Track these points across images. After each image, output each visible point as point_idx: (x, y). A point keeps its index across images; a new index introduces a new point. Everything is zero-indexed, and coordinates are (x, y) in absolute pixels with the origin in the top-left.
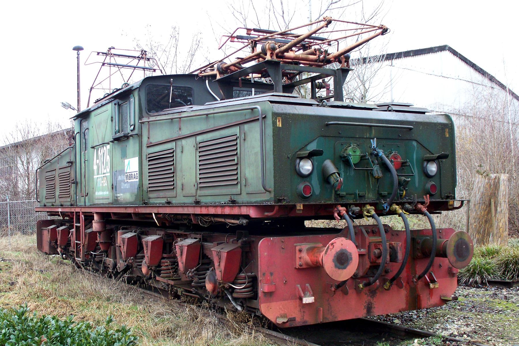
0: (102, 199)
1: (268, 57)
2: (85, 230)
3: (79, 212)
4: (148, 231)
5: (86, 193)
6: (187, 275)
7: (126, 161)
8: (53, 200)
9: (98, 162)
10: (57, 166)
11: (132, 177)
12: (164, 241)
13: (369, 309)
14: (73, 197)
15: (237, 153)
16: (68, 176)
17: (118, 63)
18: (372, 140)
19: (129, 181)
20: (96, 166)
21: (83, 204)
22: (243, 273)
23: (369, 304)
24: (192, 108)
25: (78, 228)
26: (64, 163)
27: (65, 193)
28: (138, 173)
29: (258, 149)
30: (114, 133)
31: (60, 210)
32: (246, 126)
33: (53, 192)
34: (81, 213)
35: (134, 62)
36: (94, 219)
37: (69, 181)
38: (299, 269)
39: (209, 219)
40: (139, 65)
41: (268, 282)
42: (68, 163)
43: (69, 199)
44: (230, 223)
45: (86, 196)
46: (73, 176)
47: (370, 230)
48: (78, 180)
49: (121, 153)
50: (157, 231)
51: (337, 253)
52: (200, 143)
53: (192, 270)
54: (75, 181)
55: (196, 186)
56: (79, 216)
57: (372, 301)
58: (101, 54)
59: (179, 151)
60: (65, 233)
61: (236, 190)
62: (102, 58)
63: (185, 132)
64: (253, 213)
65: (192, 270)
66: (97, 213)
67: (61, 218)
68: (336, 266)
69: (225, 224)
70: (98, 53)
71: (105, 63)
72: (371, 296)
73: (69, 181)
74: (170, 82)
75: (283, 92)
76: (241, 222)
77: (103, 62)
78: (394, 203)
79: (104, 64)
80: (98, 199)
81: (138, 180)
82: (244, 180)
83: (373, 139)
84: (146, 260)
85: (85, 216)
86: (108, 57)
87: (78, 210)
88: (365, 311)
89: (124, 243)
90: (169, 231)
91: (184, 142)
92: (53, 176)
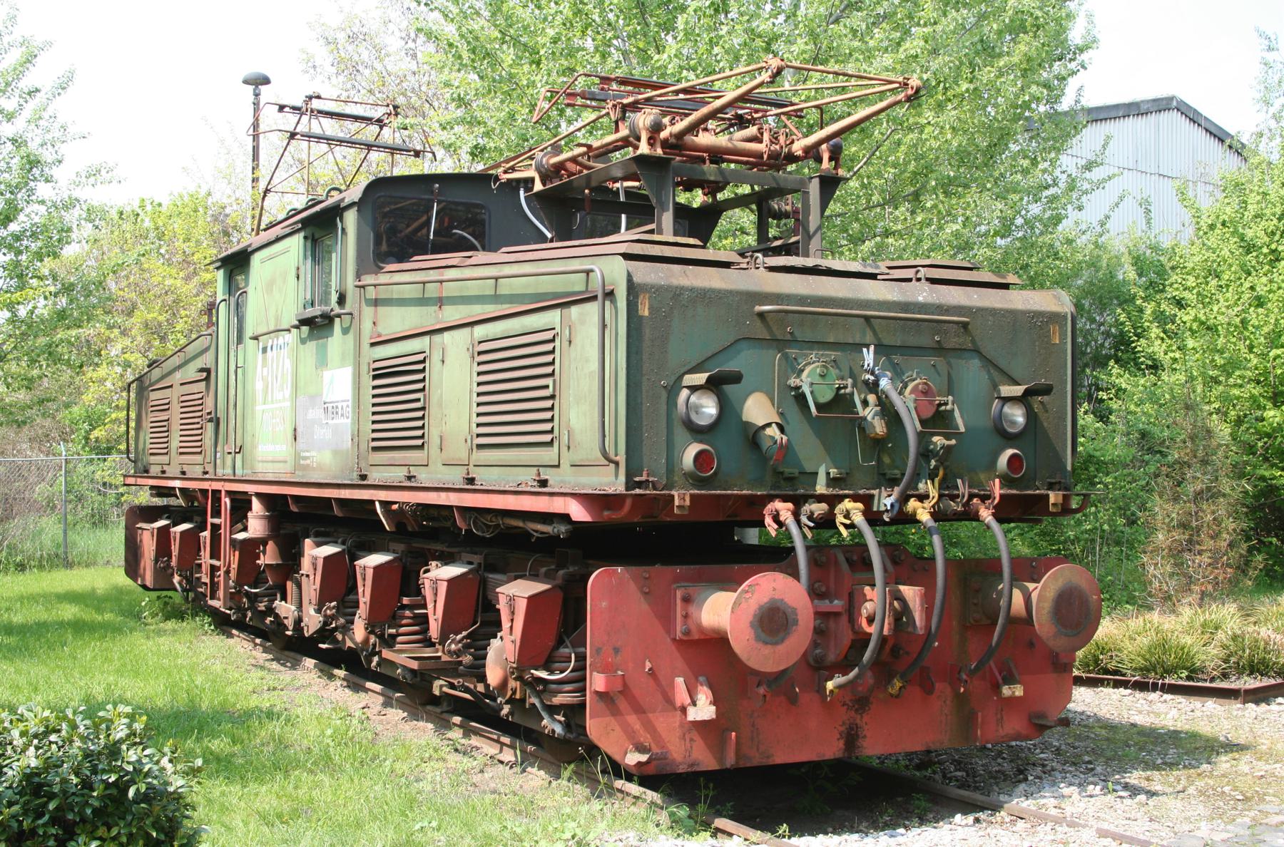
0: (273, 462)
1: (644, 148)
2: (231, 534)
3: (220, 491)
4: (374, 542)
5: (238, 444)
6: (446, 648)
7: (327, 374)
8: (165, 459)
9: (265, 373)
10: (178, 377)
11: (337, 413)
12: (404, 568)
13: (851, 738)
14: (208, 453)
15: (554, 371)
16: (200, 402)
17: (329, 133)
18: (865, 350)
19: (330, 422)
20: (261, 382)
21: (229, 471)
22: (567, 647)
23: (851, 729)
24: (470, 257)
25: (216, 528)
26: (191, 372)
27: (193, 447)
28: (350, 403)
29: (594, 366)
30: (301, 306)
31: (177, 484)
32: (574, 310)
33: (165, 440)
34: (223, 493)
35: (370, 132)
36: (251, 509)
37: (200, 414)
38: (681, 641)
39: (494, 519)
40: (381, 141)
41: (606, 669)
42: (202, 370)
43: (199, 458)
44: (536, 531)
45: (236, 453)
46: (209, 404)
47: (855, 558)
48: (221, 414)
49: (317, 354)
50: (391, 544)
51: (761, 607)
52: (480, 342)
53: (459, 637)
54: (213, 415)
55: (469, 441)
56: (219, 500)
57: (858, 721)
58: (287, 109)
59: (436, 358)
60: (190, 541)
61: (548, 455)
62: (289, 121)
63: (453, 314)
64: (579, 513)
65: (459, 637)
66: (258, 495)
67: (181, 502)
68: (758, 638)
69: (527, 535)
70: (282, 108)
71: (296, 134)
72: (857, 711)
73: (200, 414)
74: (432, 192)
75: (675, 234)
76: (556, 530)
77: (291, 129)
78: (913, 496)
79: (293, 135)
80: (263, 462)
81: (349, 421)
82: (566, 433)
83: (867, 346)
84: (363, 611)
85: (232, 501)
86: (305, 119)
87: (216, 486)
88: (841, 744)
89: (315, 569)
90: (417, 545)
91: (447, 336)
92: (167, 401)
